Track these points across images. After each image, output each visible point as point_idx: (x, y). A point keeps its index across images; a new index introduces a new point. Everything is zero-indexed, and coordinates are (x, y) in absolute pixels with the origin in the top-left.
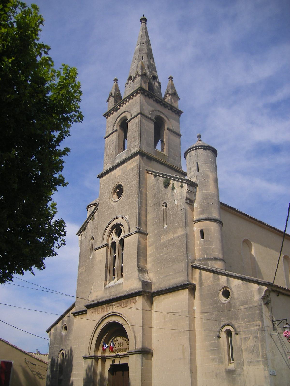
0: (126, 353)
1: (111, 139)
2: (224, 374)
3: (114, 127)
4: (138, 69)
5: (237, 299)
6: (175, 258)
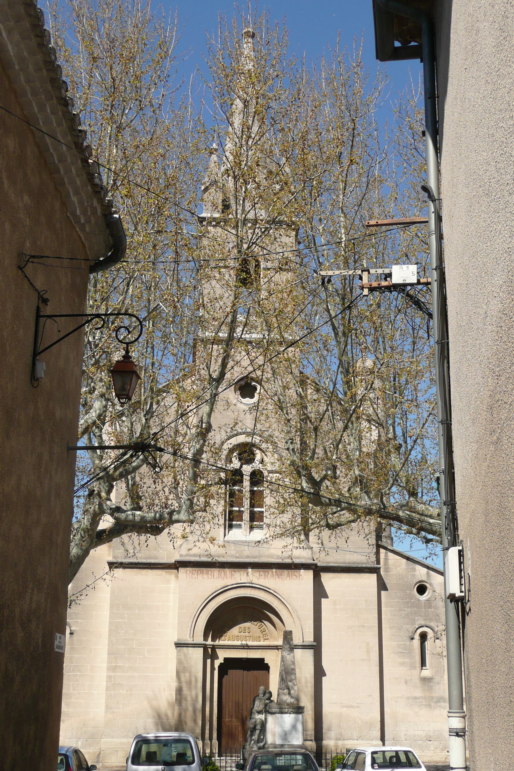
2: (418, 683)
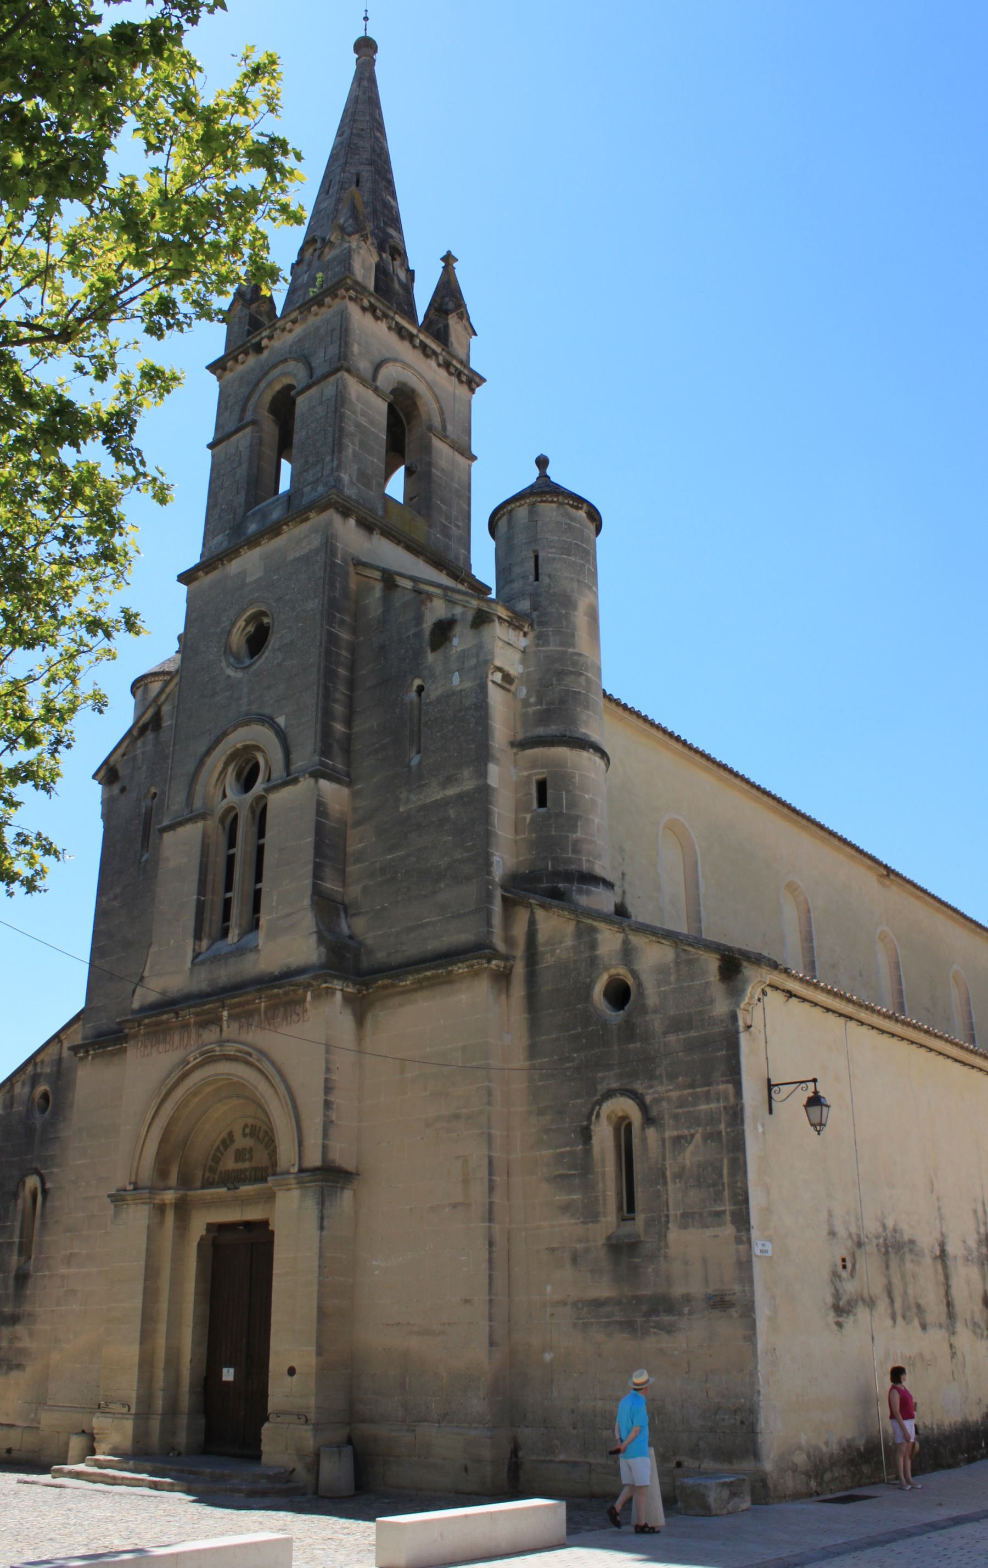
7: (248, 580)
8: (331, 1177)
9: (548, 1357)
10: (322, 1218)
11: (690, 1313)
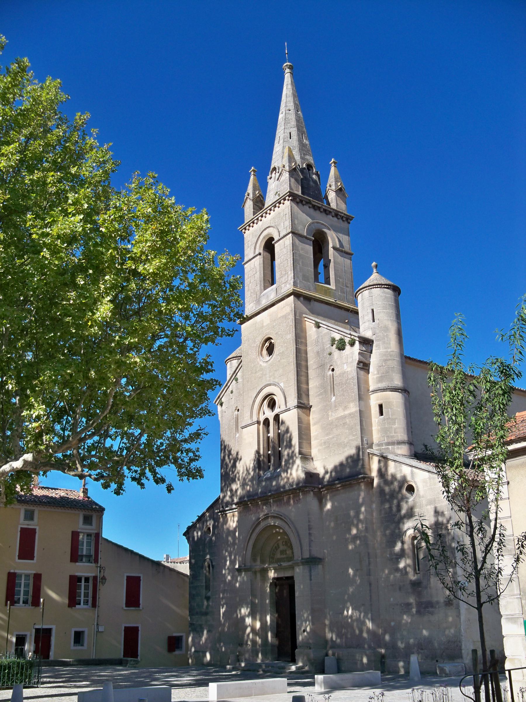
0: (290, 563)
1: (253, 266)
3: (255, 248)
4: (284, 160)
5: (423, 497)
6: (347, 443)
7: (264, 325)
8: (312, 561)
9: (393, 624)
10: (311, 576)
11: (439, 608)
